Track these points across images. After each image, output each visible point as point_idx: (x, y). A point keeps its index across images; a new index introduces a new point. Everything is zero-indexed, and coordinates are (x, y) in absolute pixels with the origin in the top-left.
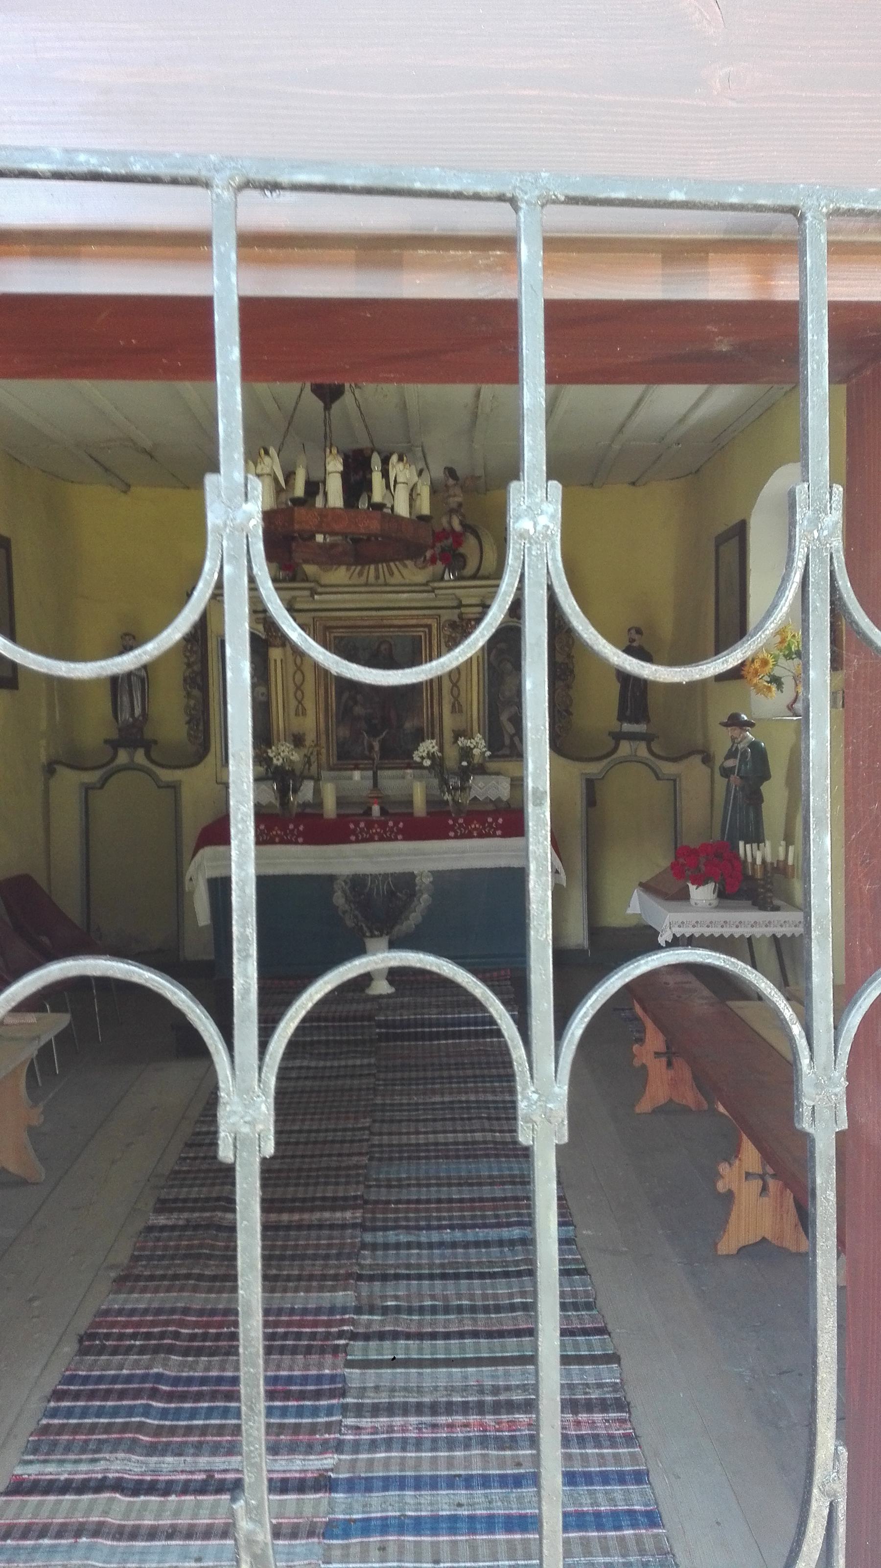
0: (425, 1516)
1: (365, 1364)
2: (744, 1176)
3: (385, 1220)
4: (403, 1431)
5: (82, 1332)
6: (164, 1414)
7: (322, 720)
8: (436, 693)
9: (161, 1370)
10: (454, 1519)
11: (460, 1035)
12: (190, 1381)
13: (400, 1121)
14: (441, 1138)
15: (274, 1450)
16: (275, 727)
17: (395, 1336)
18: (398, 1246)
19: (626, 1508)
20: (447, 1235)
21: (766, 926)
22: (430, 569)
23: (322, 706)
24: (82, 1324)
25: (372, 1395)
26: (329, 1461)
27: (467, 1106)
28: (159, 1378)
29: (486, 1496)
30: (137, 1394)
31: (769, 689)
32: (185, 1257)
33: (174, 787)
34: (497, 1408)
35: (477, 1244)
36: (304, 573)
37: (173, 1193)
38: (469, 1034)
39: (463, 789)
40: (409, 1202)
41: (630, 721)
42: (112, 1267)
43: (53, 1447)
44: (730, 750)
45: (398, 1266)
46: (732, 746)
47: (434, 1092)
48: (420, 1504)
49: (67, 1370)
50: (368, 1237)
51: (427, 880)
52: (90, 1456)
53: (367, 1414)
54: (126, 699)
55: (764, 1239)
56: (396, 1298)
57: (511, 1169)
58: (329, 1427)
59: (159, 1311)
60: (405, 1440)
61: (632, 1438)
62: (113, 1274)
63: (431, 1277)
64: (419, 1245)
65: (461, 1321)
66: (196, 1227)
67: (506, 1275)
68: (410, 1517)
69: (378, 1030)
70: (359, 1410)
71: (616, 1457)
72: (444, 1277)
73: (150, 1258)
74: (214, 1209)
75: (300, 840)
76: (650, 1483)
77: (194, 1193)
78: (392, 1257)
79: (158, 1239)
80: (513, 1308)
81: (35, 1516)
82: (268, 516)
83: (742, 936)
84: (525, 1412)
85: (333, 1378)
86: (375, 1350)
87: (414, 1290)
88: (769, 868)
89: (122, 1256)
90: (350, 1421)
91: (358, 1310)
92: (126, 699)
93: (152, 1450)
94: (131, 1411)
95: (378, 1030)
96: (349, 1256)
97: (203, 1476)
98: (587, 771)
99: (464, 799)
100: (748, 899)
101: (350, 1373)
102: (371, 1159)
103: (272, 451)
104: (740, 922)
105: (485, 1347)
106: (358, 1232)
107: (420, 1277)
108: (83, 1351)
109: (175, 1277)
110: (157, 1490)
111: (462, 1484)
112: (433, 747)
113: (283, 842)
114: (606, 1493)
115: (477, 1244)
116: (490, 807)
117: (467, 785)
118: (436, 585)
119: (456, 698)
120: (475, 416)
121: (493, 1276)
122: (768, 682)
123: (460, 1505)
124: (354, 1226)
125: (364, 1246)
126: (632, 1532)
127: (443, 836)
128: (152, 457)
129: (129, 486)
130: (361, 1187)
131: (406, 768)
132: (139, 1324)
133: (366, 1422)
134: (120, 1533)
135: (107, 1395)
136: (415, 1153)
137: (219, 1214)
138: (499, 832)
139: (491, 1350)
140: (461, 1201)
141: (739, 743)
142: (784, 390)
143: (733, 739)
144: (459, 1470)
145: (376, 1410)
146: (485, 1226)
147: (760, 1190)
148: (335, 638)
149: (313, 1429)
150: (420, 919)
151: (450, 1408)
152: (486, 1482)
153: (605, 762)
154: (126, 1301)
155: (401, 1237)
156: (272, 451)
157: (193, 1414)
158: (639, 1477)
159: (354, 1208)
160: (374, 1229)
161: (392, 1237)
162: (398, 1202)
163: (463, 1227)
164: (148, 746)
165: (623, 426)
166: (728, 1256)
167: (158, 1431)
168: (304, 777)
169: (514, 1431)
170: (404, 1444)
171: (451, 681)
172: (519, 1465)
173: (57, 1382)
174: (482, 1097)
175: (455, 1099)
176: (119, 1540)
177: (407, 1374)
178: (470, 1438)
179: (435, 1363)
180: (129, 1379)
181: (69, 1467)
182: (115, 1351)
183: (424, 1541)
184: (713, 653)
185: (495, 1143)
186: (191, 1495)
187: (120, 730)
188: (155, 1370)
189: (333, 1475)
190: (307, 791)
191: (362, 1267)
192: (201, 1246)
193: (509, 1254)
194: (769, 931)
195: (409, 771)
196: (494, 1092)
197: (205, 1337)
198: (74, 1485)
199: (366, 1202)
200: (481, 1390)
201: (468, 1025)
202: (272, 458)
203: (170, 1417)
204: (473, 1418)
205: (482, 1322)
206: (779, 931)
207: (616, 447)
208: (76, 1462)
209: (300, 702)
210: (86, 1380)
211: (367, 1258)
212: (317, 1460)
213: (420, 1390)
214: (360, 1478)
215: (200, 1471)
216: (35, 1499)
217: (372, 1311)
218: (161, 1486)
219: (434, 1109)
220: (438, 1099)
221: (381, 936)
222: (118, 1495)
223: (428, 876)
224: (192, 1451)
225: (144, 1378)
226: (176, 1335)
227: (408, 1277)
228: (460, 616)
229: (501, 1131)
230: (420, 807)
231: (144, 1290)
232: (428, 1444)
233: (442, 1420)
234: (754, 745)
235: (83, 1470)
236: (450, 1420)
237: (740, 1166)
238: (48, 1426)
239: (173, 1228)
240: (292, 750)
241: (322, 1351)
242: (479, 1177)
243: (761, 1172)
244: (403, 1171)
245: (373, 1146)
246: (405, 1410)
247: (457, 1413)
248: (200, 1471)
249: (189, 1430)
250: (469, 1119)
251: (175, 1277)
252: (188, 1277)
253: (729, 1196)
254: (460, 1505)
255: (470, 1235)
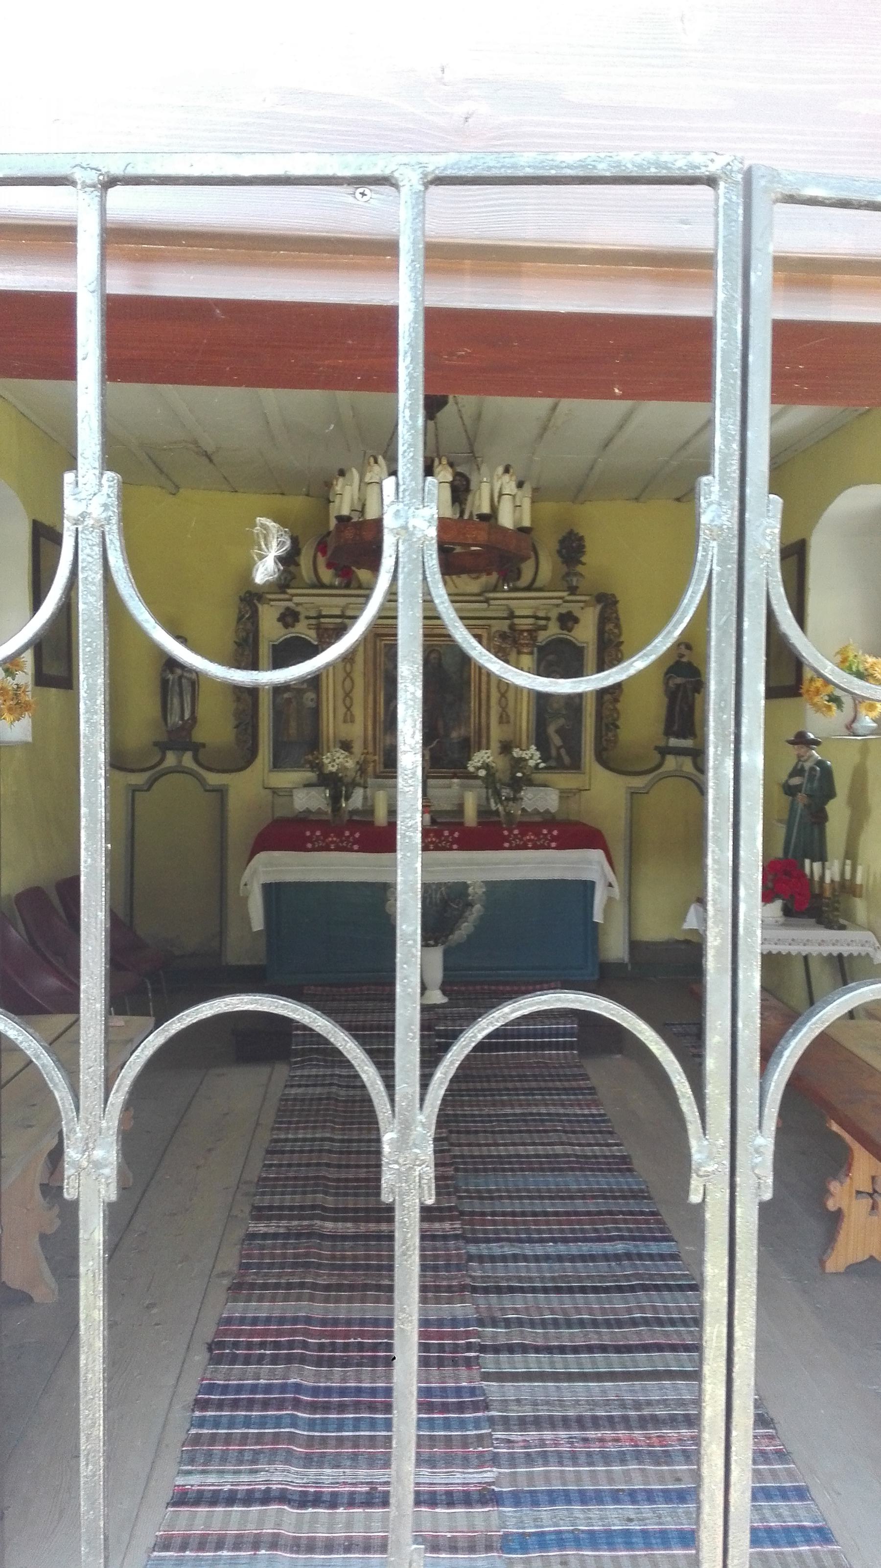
0: (598, 1531)
1: (501, 1377)
2: (854, 1194)
3: (485, 1232)
4: (556, 1445)
5: (209, 1341)
6: (311, 1425)
7: (370, 727)
8: (484, 702)
9: (298, 1380)
10: (627, 1533)
11: (518, 1047)
12: (328, 1391)
13: (476, 1132)
14: (521, 1150)
15: (420, 1462)
16: (325, 733)
17: (524, 1349)
18: (504, 1258)
19: (795, 1523)
20: (551, 1248)
21: (834, 945)
22: (484, 579)
23: (370, 711)
24: (208, 1332)
25: (515, 1408)
26: (489, 1474)
27: (541, 1119)
28: (298, 1388)
29: (654, 1511)
30: (281, 1404)
31: (829, 708)
32: (295, 1265)
33: (221, 792)
34: (644, 1422)
35: (583, 1258)
36: (359, 581)
37: (266, 1201)
38: (528, 1046)
39: (515, 799)
40: (504, 1214)
41: (678, 736)
42: (223, 1274)
43: (209, 1457)
44: (795, 768)
45: (509, 1279)
46: (797, 764)
47: (503, 1104)
48: (590, 1518)
49: (203, 1380)
50: (473, 1249)
51: (481, 891)
52: (201, 1468)
53: (516, 1427)
54: (176, 701)
55: (872, 1258)
56: (516, 1311)
57: (598, 1183)
58: (480, 1439)
59: (281, 1320)
60: (559, 1454)
61: (785, 1455)
62: (226, 1282)
63: (545, 1290)
64: (526, 1258)
65: (586, 1335)
66: (298, 1236)
67: (620, 1289)
68: (583, 1531)
69: (437, 1040)
70: (506, 1423)
71: (773, 1472)
72: (558, 1290)
73: (259, 1266)
74: (311, 1218)
75: (356, 847)
76: (813, 1500)
77: (288, 1200)
78: (500, 1271)
79: (262, 1247)
80: (634, 1323)
81: (208, 1527)
82: (443, 524)
83: (799, 953)
84: (672, 1428)
85: (472, 1391)
86: (507, 1363)
87: (531, 1304)
88: (837, 886)
89: (230, 1262)
90: (499, 1435)
91: (481, 1322)
92: (176, 701)
93: (308, 1461)
94: (278, 1422)
95: (437, 1040)
96: (459, 1268)
97: (365, 1489)
98: (633, 785)
99: (515, 810)
100: (811, 917)
101: (487, 1385)
102: (457, 1170)
103: (380, 459)
104: (808, 940)
105: (616, 1362)
106: (461, 1243)
107: (534, 1290)
108: (217, 1360)
109: (289, 1286)
110: (324, 1502)
111: (627, 1498)
112: (488, 757)
113: (339, 849)
114: (772, 1508)
115: (583, 1258)
116: (537, 819)
117: (518, 796)
118: (491, 595)
119: (504, 709)
120: (545, 429)
121: (607, 1290)
122: (828, 701)
123: (630, 1520)
124: (456, 1237)
125: (470, 1258)
126: (807, 1548)
127: (498, 847)
128: (211, 461)
129: (177, 487)
130: (454, 1198)
131: (452, 777)
132: (265, 1333)
133: (516, 1436)
134: (296, 1546)
135: (250, 1404)
136: (500, 1164)
137: (318, 1222)
138: (553, 845)
139: (610, 1365)
140: (556, 1214)
141: (806, 761)
142: (858, 413)
143: (799, 757)
144: (620, 1484)
145: (523, 1423)
146: (586, 1240)
147: (869, 1209)
148: (386, 645)
149: (465, 1442)
150: (472, 929)
151: (596, 1423)
152: (650, 1496)
153: (647, 779)
154: (245, 1310)
155: (506, 1249)
156: (380, 459)
157: (341, 1425)
158: (801, 1493)
159: (452, 1219)
160: (476, 1241)
161: (496, 1249)
162: (494, 1214)
163: (565, 1241)
164: (196, 748)
165: (688, 443)
166: (836, 1274)
167: (310, 1442)
168: (354, 784)
169: (665, 1446)
170: (560, 1459)
171: (499, 691)
172: (678, 1480)
173: (196, 1392)
174: (553, 1110)
175: (525, 1111)
176: (297, 1552)
177: (545, 1387)
178: (623, 1453)
179: (570, 1377)
180: (268, 1389)
181: (230, 1478)
182: (247, 1360)
183: (603, 1556)
184: (595, 669)
185: (577, 1156)
186: (359, 1507)
187: (170, 732)
188: (292, 1380)
189: (496, 1489)
190: (357, 800)
191: (473, 1278)
192: (307, 1255)
193: (617, 1268)
194: (826, 950)
195: (456, 780)
196: (563, 1105)
197: (333, 1347)
198: (239, 1496)
199: (462, 1213)
200: (623, 1405)
201: (527, 1037)
202: (380, 466)
203: (318, 1427)
204: (621, 1433)
205: (606, 1336)
206: (845, 950)
207: (674, 463)
208: (236, 1472)
209: (348, 709)
210: (225, 1389)
211: (477, 1270)
212: (477, 1473)
213: (561, 1403)
214: (523, 1491)
215: (362, 1483)
216: (203, 1510)
217: (494, 1323)
218: (326, 1498)
219: (508, 1121)
220: (509, 1111)
221: (436, 945)
222: (286, 1507)
223: (481, 887)
224: (348, 1463)
225: (283, 1388)
226: (305, 1345)
227: (522, 1290)
228: (512, 627)
229: (579, 1145)
230: (470, 817)
231: (261, 1299)
232: (583, 1459)
233: (592, 1434)
234: (820, 763)
235: (244, 1481)
236: (599, 1434)
237: (851, 1185)
238: (198, 1436)
239: (275, 1236)
240: (346, 757)
241: (455, 1362)
242: (568, 1190)
243: (871, 1191)
244: (492, 1183)
245: (455, 1157)
246: (552, 1423)
247: (605, 1428)
248: (362, 1483)
249: (340, 1442)
250: (546, 1131)
251: (289, 1286)
252: (302, 1285)
253: (837, 1216)
254: (630, 1520)
255: (574, 1249)
